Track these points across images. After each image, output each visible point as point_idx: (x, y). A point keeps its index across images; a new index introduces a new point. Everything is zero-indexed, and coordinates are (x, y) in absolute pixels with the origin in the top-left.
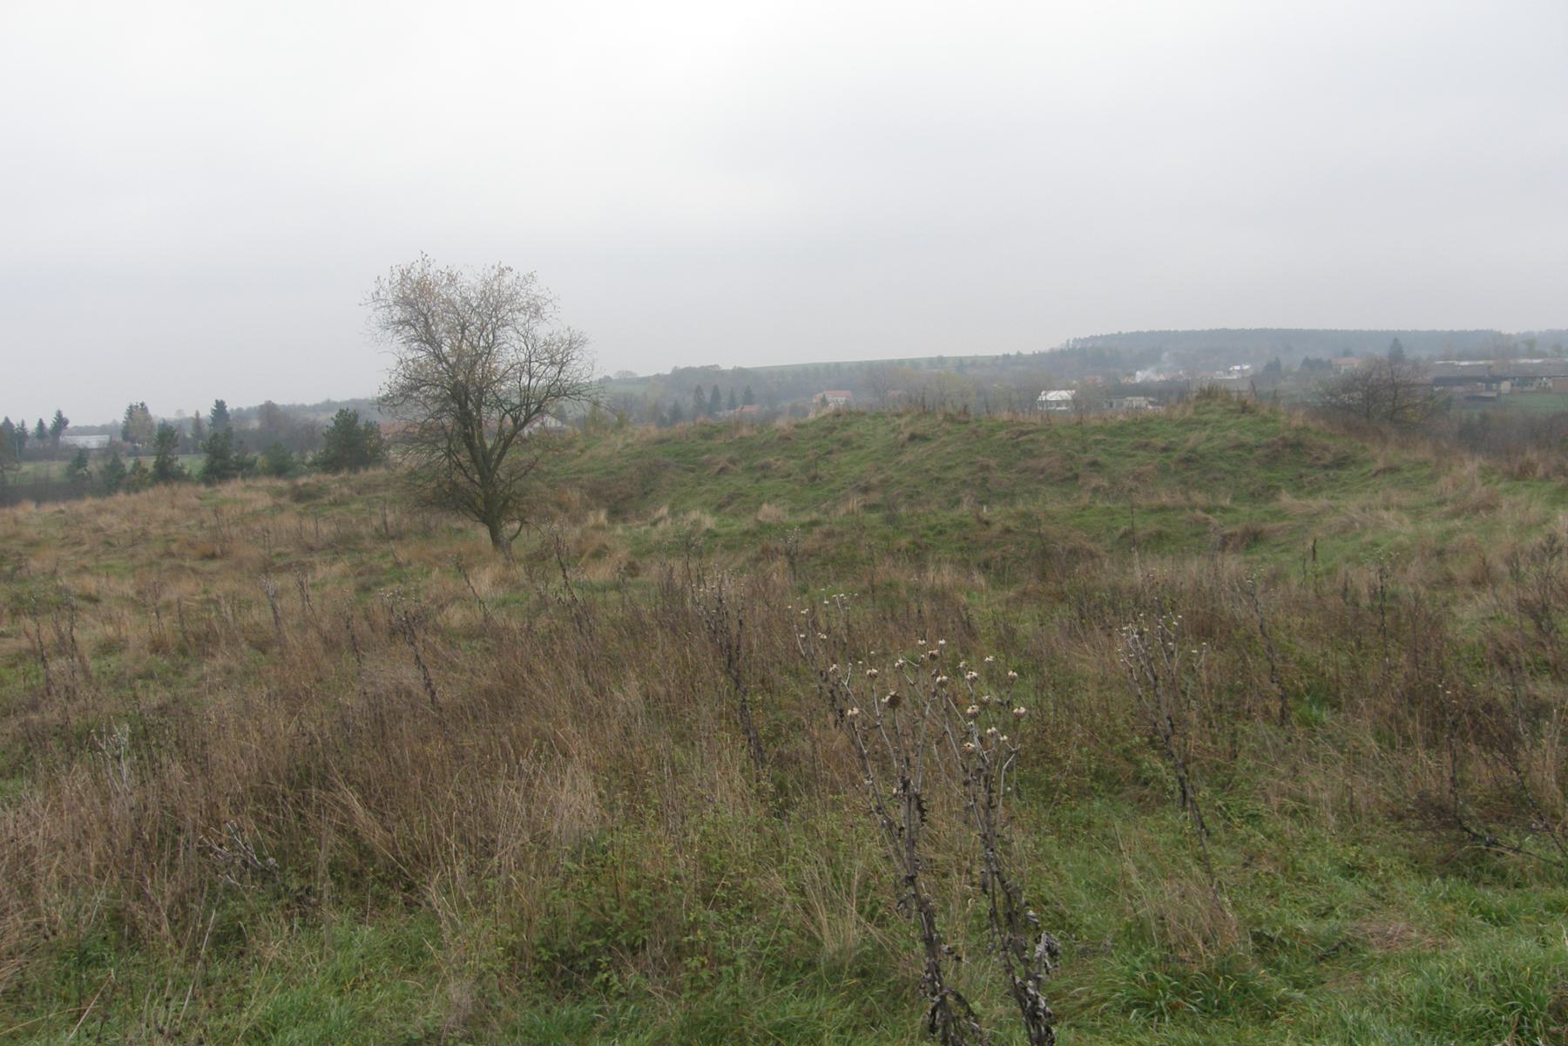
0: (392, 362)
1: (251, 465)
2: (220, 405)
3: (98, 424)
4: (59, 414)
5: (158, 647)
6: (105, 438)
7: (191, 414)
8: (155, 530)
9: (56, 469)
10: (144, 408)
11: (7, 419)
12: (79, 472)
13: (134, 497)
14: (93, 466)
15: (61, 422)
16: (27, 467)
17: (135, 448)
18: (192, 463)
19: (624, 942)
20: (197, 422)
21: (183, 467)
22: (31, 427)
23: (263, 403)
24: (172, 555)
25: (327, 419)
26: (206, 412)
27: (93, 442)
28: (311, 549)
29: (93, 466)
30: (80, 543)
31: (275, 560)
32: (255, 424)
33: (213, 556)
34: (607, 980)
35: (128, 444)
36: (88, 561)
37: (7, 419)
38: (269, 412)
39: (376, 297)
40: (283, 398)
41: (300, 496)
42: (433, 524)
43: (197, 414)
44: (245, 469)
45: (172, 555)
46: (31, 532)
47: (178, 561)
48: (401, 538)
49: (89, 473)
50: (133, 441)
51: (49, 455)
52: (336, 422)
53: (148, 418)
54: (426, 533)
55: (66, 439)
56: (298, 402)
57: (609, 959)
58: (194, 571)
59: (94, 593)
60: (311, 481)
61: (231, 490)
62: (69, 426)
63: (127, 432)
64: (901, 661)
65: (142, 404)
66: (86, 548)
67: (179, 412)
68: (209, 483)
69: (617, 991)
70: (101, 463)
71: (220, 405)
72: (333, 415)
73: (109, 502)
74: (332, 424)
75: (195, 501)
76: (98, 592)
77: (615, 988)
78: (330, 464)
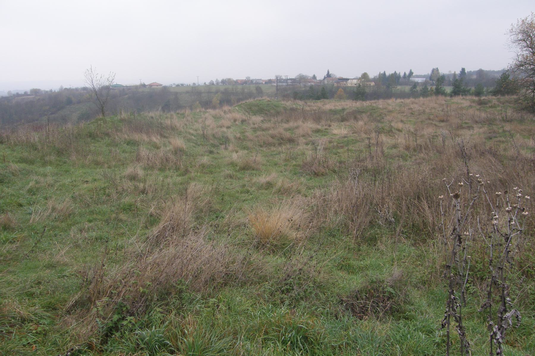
0: (514, 55)
1: (468, 91)
2: (463, 70)
3: (423, 74)
4: (411, 71)
5: (407, 148)
6: (424, 79)
7: (453, 72)
8: (427, 111)
9: (407, 89)
10: (437, 69)
11: (395, 72)
12: (414, 90)
13: (425, 99)
14: (418, 88)
15: (411, 73)
16: (399, 87)
17: (433, 83)
18: (448, 89)
19: (478, 276)
20: (455, 75)
21: (445, 90)
22: (402, 74)
23: (478, 69)
24: (430, 119)
25: (498, 76)
26: (458, 72)
27: (420, 80)
28: (477, 122)
29: (418, 88)
30: (403, 113)
31: (463, 125)
32: (475, 77)
33: (443, 121)
34: (469, 287)
35: (431, 81)
36: (404, 119)
37: (395, 72)
38: (480, 73)
39: (511, 31)
40: (486, 67)
41: (481, 103)
42: (525, 117)
43: (455, 72)
44: (465, 92)
45: (430, 119)
46: (390, 108)
47: (431, 122)
48: (511, 122)
49: (417, 90)
50: (433, 81)
51: (406, 84)
52: (501, 77)
53: (438, 73)
54: (522, 121)
55: (412, 79)
56: (492, 70)
57: (472, 280)
58: (435, 125)
59: (400, 129)
60: (486, 98)
61: (457, 99)
62: (414, 75)
63: (431, 78)
64: (462, 183)
65: (437, 68)
66: (405, 114)
67: (450, 71)
68: (451, 96)
69: (470, 292)
70: (421, 87)
71: (463, 70)
72: (500, 74)
73: (417, 100)
74: (500, 78)
75: (444, 102)
76: (402, 129)
77: (469, 290)
78: (495, 93)
